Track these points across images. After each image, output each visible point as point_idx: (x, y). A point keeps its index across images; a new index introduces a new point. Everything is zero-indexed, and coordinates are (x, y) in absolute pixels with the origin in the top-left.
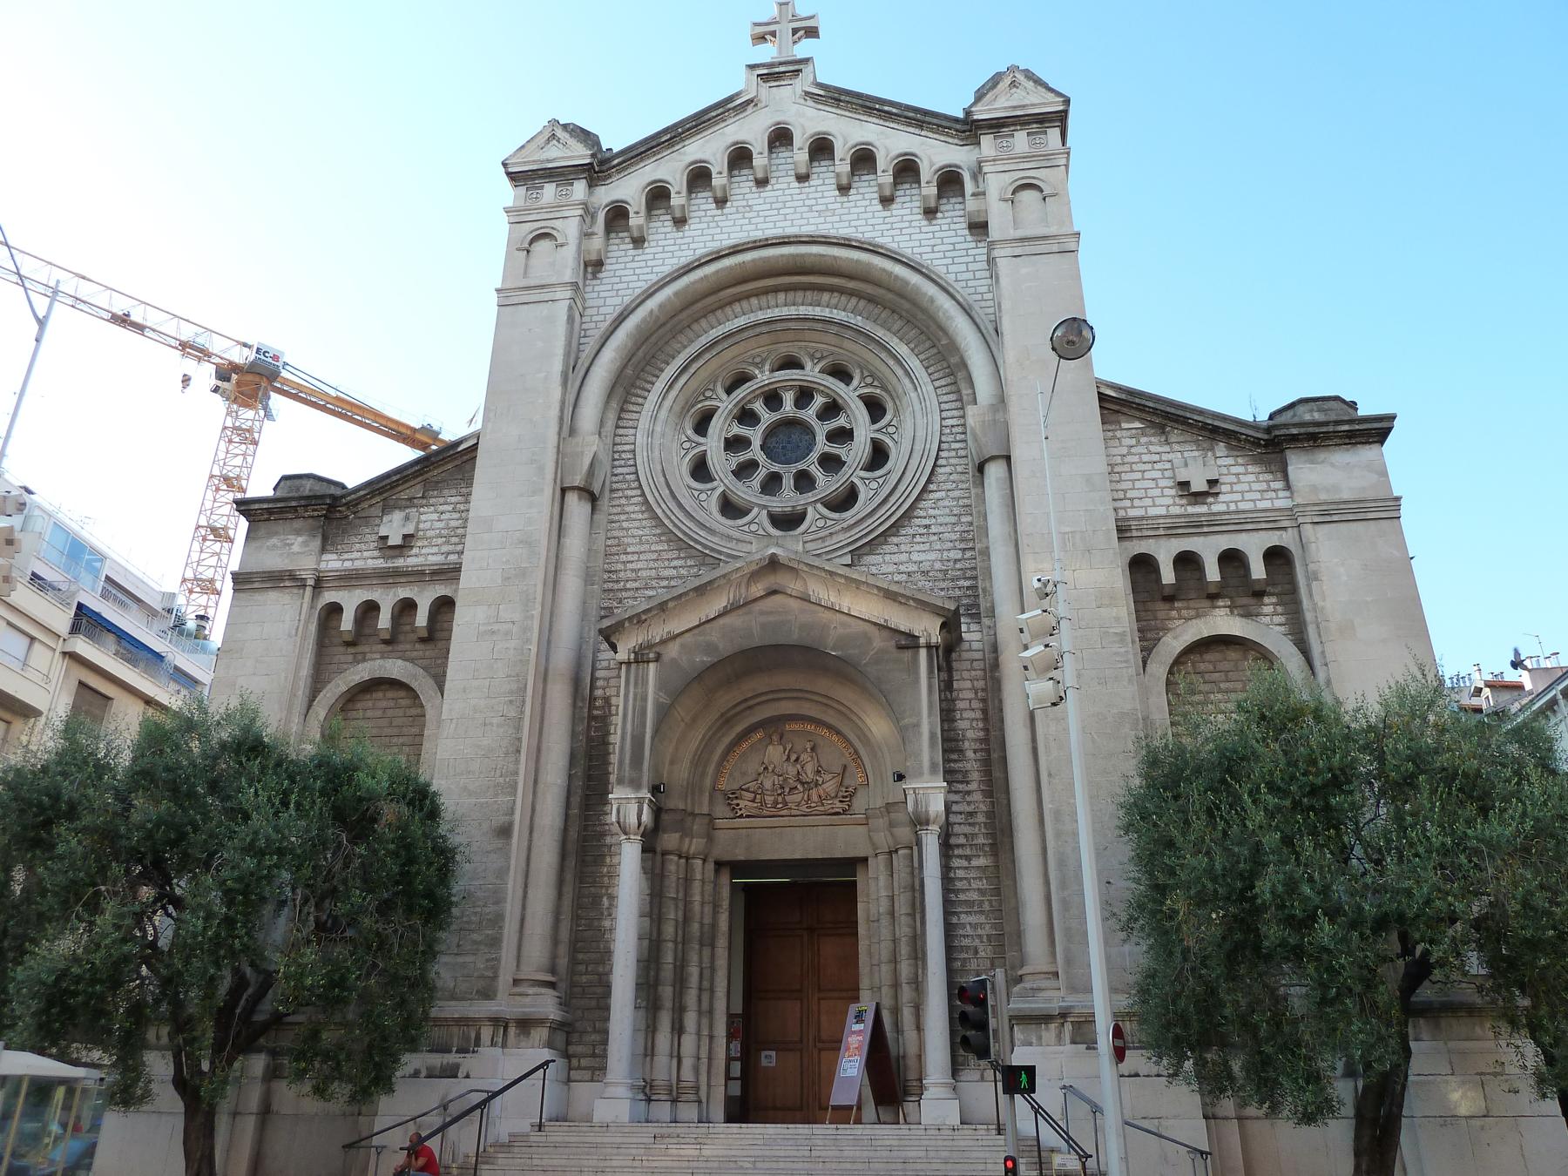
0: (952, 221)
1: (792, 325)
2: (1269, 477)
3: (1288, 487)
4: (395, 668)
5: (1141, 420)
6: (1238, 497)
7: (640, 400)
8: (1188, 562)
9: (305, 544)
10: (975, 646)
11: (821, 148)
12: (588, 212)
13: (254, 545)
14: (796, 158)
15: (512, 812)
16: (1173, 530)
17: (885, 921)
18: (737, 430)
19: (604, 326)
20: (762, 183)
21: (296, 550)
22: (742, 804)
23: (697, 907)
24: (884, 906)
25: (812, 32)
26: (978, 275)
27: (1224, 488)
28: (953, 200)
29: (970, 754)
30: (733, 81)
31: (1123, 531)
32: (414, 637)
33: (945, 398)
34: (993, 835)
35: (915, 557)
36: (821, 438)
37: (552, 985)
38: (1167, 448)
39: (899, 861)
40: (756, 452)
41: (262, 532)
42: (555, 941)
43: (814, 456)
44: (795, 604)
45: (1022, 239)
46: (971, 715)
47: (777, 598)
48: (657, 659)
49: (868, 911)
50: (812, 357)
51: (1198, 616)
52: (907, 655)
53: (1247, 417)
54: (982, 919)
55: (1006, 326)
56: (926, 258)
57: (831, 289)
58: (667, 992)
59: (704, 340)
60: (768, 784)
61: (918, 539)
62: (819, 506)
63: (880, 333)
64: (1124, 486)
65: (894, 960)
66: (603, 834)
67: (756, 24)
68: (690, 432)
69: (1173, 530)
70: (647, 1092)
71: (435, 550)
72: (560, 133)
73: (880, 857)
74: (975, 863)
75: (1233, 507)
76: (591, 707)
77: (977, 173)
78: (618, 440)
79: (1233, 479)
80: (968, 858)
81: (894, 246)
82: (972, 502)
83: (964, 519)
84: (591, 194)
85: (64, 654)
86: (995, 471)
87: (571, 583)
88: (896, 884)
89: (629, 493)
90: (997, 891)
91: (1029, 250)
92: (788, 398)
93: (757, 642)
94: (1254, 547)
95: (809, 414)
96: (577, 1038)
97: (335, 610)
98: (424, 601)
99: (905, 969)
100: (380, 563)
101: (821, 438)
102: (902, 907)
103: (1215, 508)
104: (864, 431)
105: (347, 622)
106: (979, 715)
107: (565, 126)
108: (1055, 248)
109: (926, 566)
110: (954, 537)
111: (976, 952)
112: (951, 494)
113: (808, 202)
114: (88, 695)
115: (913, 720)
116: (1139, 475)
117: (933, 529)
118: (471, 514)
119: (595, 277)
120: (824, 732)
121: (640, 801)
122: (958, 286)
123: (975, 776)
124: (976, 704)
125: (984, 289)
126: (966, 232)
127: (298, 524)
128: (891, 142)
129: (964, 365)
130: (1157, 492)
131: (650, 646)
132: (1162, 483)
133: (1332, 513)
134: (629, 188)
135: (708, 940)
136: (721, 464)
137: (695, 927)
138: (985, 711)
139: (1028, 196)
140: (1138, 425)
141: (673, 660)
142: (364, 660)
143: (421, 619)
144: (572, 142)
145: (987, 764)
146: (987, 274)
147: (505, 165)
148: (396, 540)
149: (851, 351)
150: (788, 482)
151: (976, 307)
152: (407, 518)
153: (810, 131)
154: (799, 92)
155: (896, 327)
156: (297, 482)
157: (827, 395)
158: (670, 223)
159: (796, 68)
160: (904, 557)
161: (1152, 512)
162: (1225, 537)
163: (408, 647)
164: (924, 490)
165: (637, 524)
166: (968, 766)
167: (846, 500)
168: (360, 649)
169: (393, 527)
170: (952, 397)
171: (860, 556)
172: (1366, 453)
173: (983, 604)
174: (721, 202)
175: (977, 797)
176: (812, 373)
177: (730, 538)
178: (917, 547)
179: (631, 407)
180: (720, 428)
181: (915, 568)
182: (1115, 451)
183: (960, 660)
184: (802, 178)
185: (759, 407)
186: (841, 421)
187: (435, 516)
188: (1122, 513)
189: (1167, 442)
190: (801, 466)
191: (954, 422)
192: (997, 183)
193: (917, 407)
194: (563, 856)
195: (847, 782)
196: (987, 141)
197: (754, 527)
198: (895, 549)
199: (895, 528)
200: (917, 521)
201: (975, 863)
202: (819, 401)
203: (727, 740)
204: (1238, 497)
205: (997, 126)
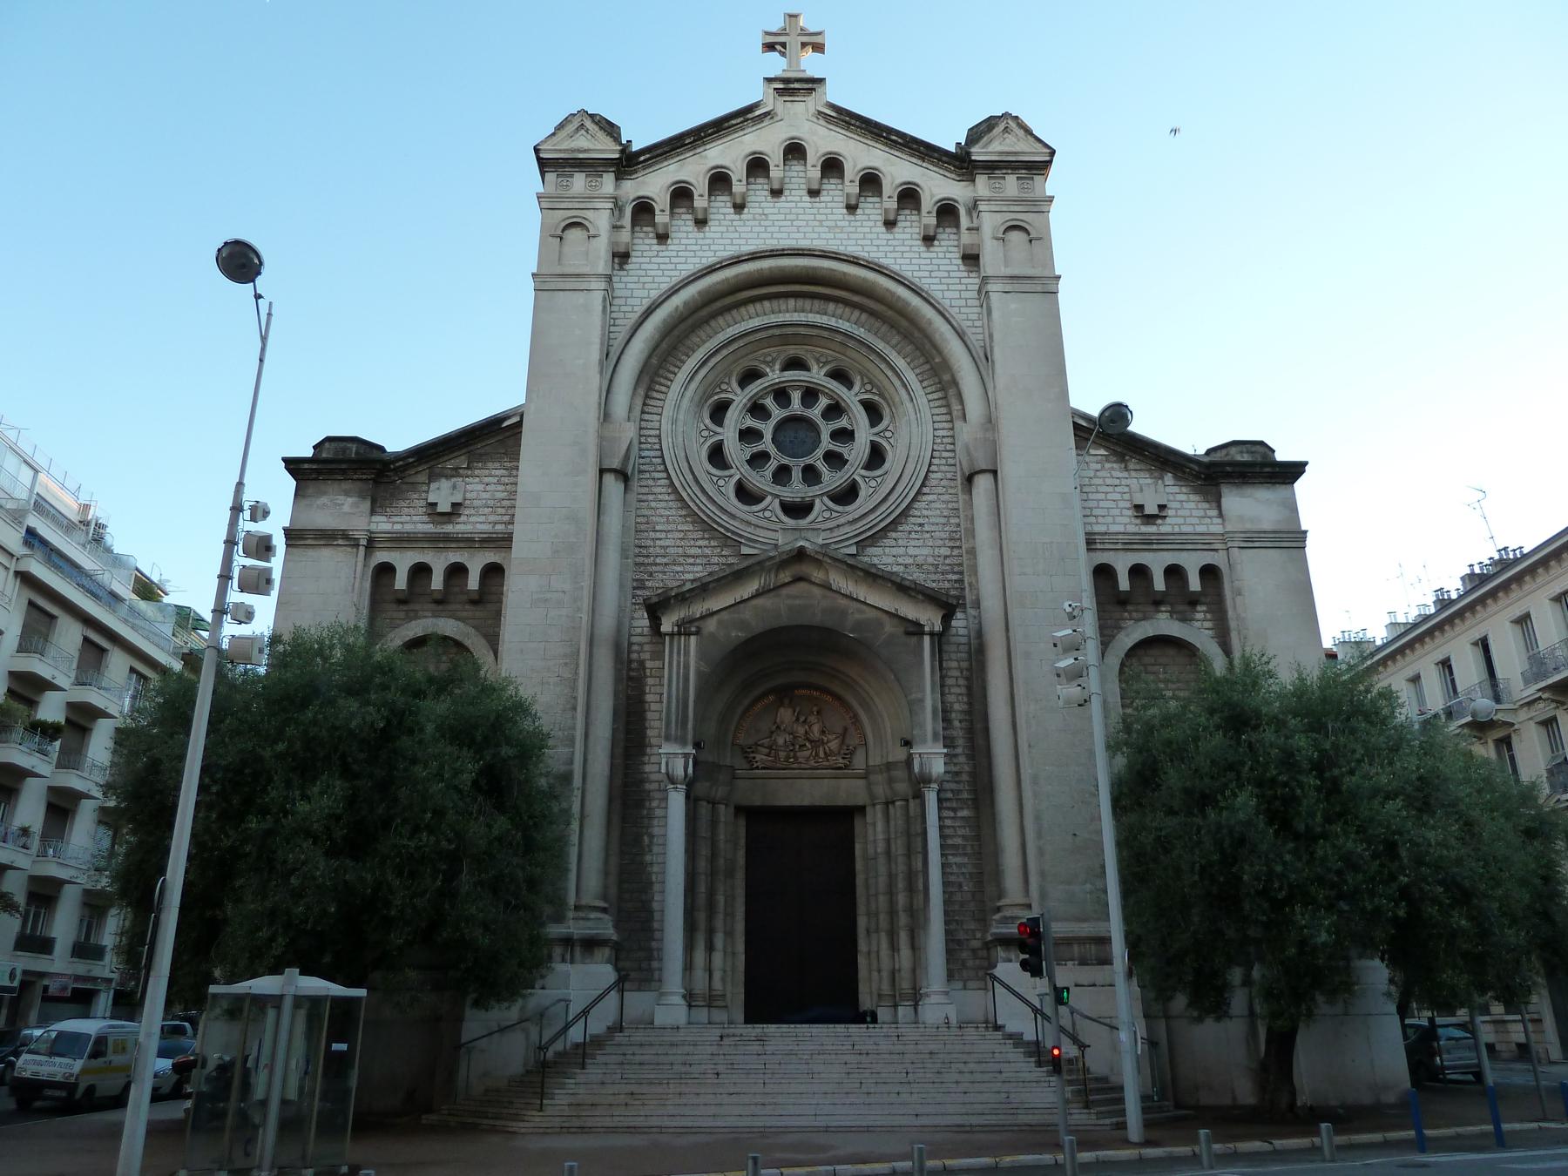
0: (948, 249)
1: (802, 331)
2: (1206, 505)
3: (1221, 515)
4: (448, 626)
5: (1106, 448)
6: (1181, 521)
7: (663, 389)
8: (1139, 572)
9: (355, 505)
10: (962, 631)
11: (832, 166)
12: (618, 207)
13: (304, 502)
14: (809, 174)
15: (571, 762)
16: (1128, 546)
17: (882, 860)
18: (750, 422)
19: (635, 317)
20: (777, 193)
21: (343, 508)
22: (759, 757)
23: (722, 845)
24: (881, 848)
25: (819, 48)
26: (970, 302)
27: (1170, 512)
28: (948, 230)
29: (957, 723)
30: (751, 91)
31: (1091, 543)
32: (465, 597)
33: (936, 411)
34: (974, 791)
35: (911, 551)
36: (825, 437)
37: (604, 910)
38: (1125, 474)
39: (897, 811)
40: (767, 444)
41: (310, 491)
42: (606, 874)
43: (820, 452)
44: (816, 591)
45: (1012, 277)
46: (957, 690)
47: (802, 586)
48: (697, 633)
49: (865, 850)
50: (818, 361)
51: (1144, 619)
52: (914, 639)
53: (1190, 452)
54: (966, 860)
55: (998, 355)
56: (925, 283)
57: (836, 300)
58: (701, 917)
59: (721, 337)
60: (781, 741)
61: (913, 535)
62: (825, 499)
63: (880, 345)
64: (1091, 504)
65: (891, 893)
66: (642, 781)
67: (767, 33)
68: (708, 421)
69: (1128, 546)
70: (690, 998)
71: (482, 519)
72: (588, 124)
73: (878, 807)
74: (960, 814)
75: (1177, 529)
76: (630, 669)
77: (973, 207)
78: (644, 424)
79: (1177, 505)
80: (954, 810)
81: (896, 268)
82: (961, 505)
83: (952, 521)
84: (617, 187)
85: (17, 573)
86: (983, 483)
87: (612, 557)
88: (892, 829)
89: (657, 475)
90: (978, 837)
91: (1017, 287)
92: (796, 397)
93: (784, 622)
94: (1192, 563)
95: (815, 413)
96: (634, 960)
97: (386, 570)
98: (475, 565)
99: (901, 899)
100: (430, 528)
101: (825, 437)
102: (899, 848)
103: (1164, 529)
104: (864, 435)
105: (401, 582)
106: (963, 690)
107: (592, 116)
108: (1039, 289)
109: (920, 560)
110: (943, 535)
111: (960, 885)
112: (943, 498)
113: (819, 217)
114: (35, 614)
115: (919, 696)
116: (1102, 496)
117: (926, 528)
118: (520, 489)
119: (621, 269)
120: (829, 699)
121: (686, 756)
122: (954, 311)
123: (960, 742)
124: (962, 682)
125: (975, 317)
126: (960, 261)
127: (347, 485)
128: (898, 170)
129: (955, 383)
130: (1117, 512)
131: (692, 621)
132: (1121, 504)
133: (1253, 540)
134: (655, 184)
135: (730, 874)
136: (736, 452)
137: (721, 861)
138: (969, 688)
139: (1015, 236)
140: (1102, 452)
141: (712, 635)
142: (417, 618)
143: (473, 582)
144: (601, 135)
145: (970, 732)
146: (977, 303)
147: (537, 150)
148: (444, 507)
149: (851, 360)
150: (797, 474)
151: (969, 331)
152: (454, 487)
153: (823, 150)
154: (812, 110)
155: (894, 342)
156: (342, 445)
157: (831, 398)
158: (691, 223)
159: (813, 84)
160: (901, 551)
161: (1114, 529)
162: (1170, 554)
163: (458, 607)
164: (919, 493)
165: (663, 504)
166: (955, 733)
167: (847, 495)
168: (411, 606)
169: (442, 494)
170: (943, 410)
171: (864, 547)
172: (1279, 492)
173: (969, 597)
174: (739, 207)
175: (962, 759)
176: (817, 375)
177: (749, 523)
178: (913, 543)
179: (655, 395)
180: (735, 418)
181: (911, 561)
182: (1085, 473)
183: (949, 643)
184: (814, 193)
185: (769, 402)
186: (843, 423)
187: (481, 487)
188: (1089, 528)
189: (1126, 469)
190: (808, 460)
191: (944, 433)
192: (990, 222)
193: (913, 417)
194: (610, 800)
195: (847, 741)
196: (981, 180)
197: (767, 514)
198: (893, 543)
199: (894, 525)
200: (912, 520)
201: (960, 814)
202: (824, 401)
203: (746, 702)
204: (1181, 521)
205: (991, 167)
